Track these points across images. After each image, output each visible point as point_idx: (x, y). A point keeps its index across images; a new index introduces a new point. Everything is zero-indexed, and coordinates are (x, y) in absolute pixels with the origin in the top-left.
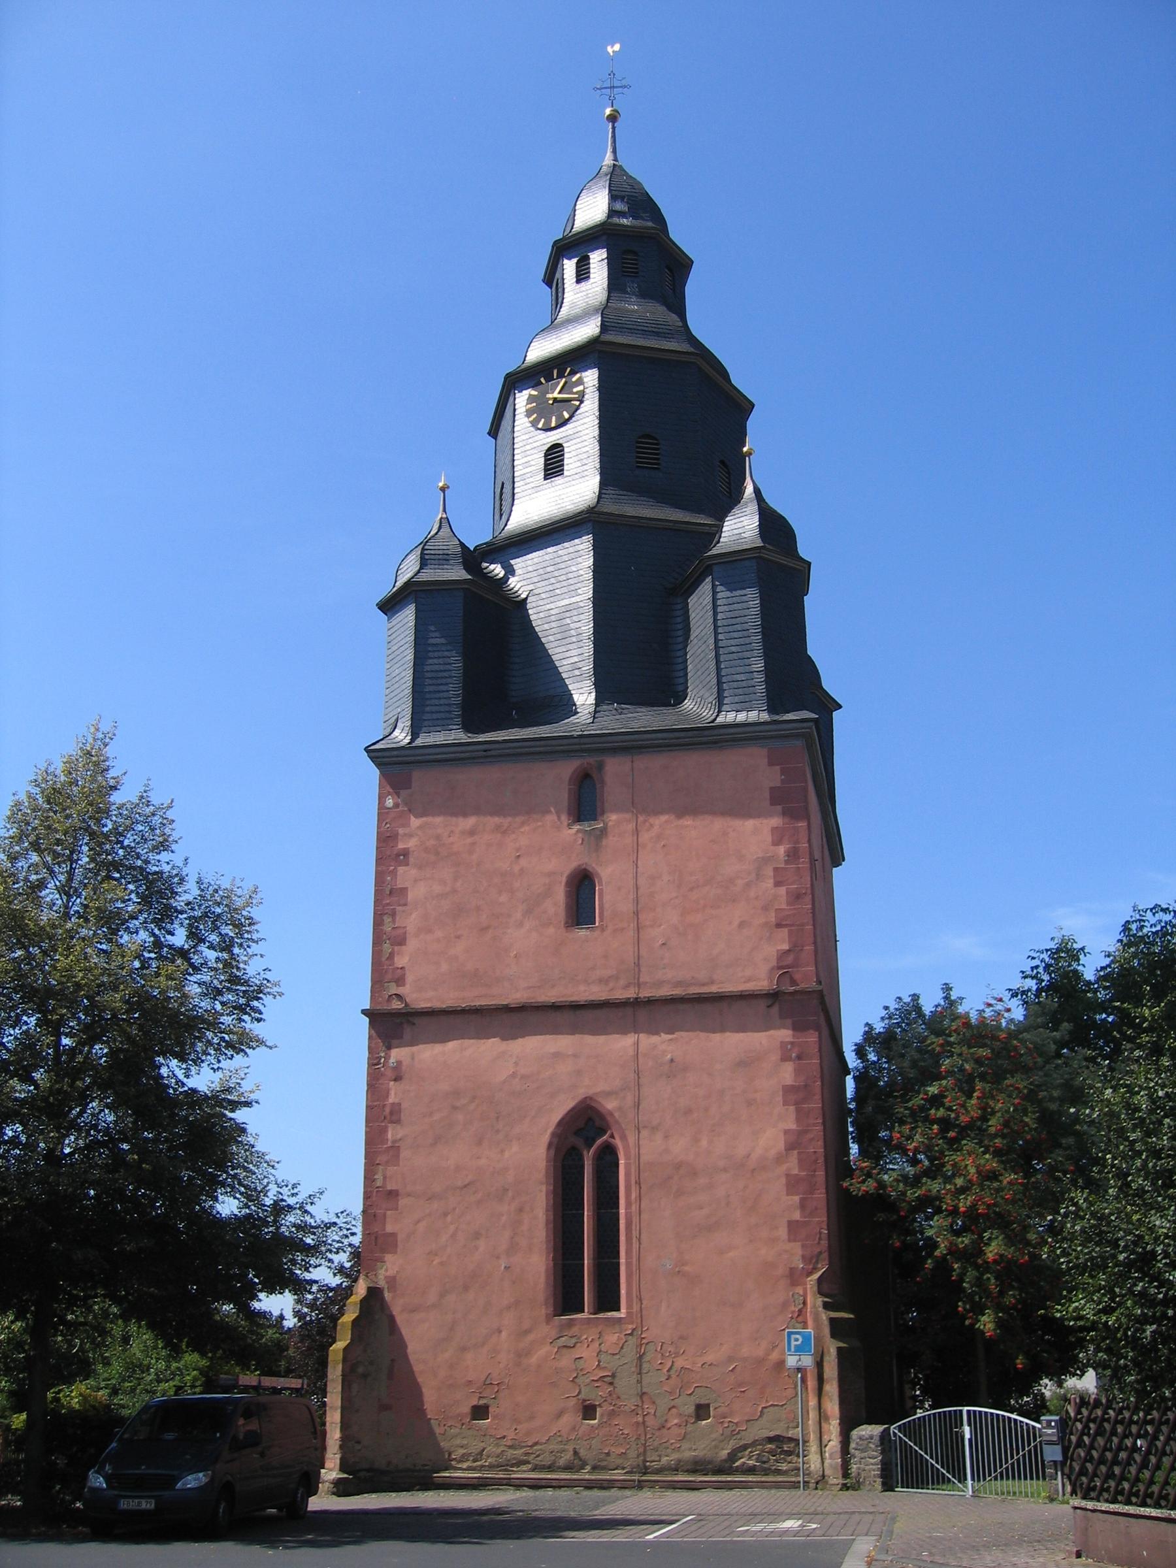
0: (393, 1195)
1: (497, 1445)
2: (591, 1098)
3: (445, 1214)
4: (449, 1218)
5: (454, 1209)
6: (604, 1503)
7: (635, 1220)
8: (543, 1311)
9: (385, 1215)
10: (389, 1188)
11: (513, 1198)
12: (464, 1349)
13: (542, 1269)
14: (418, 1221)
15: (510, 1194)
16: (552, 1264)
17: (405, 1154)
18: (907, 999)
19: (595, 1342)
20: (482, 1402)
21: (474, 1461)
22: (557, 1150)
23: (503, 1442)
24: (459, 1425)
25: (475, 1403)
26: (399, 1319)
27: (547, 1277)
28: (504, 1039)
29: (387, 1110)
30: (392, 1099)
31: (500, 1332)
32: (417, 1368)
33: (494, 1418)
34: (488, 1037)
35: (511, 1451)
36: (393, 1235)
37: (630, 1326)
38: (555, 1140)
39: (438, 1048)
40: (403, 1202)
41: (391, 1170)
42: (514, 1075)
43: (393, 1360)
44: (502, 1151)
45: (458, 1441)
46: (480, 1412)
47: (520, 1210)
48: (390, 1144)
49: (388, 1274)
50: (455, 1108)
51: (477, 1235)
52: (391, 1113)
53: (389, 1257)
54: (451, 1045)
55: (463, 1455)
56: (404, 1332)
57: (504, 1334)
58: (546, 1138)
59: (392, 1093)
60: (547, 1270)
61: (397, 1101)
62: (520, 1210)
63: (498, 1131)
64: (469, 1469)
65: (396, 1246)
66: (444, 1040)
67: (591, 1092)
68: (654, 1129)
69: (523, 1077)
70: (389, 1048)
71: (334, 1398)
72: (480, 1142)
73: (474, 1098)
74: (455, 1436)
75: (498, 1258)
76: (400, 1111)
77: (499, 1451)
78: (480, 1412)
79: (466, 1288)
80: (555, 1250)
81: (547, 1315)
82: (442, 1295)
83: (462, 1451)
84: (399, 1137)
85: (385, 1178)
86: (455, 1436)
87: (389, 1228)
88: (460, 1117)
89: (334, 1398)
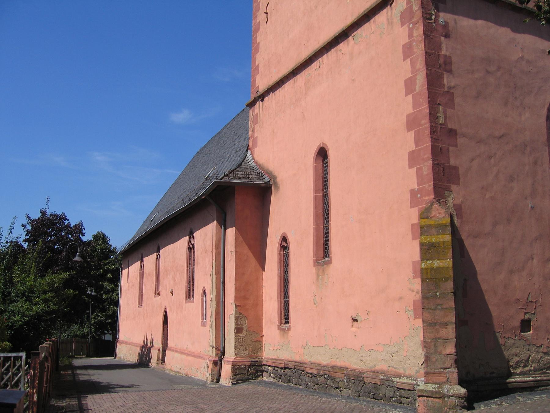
0: (452, 133)
1: (538, 352)
3: (490, 157)
4: (493, 160)
5: (495, 154)
6: (94, 374)
9: (448, 151)
10: (450, 126)
12: (511, 272)
14: (473, 160)
15: (528, 149)
17: (457, 100)
18: (83, 231)
19: (141, 309)
20: (527, 317)
21: (525, 366)
23: (541, 349)
24: (513, 337)
25: (523, 318)
26: (467, 243)
28: (514, 31)
29: (442, 60)
30: (444, 52)
31: (533, 259)
32: (484, 287)
33: (534, 330)
34: (502, 25)
35: (546, 357)
36: (456, 168)
39: (471, 22)
40: (461, 141)
41: (449, 111)
42: (522, 58)
43: (465, 280)
44: (520, 115)
45: (513, 351)
46: (526, 325)
48: (446, 89)
49: (455, 202)
50: (488, 72)
51: (511, 179)
52: (445, 63)
53: (453, 187)
54: (480, 22)
55: (517, 362)
56: (471, 255)
57: (535, 261)
59: (444, 46)
61: (448, 54)
62: (535, 163)
64: (522, 374)
65: (459, 179)
66: (476, 19)
69: (528, 61)
70: (438, 9)
72: (506, 104)
73: (499, 68)
74: (511, 347)
75: (526, 198)
76: (450, 63)
77: (539, 357)
78: (526, 325)
79: (509, 221)
82: (495, 225)
83: (516, 359)
84: (452, 84)
85: (446, 117)
86: (511, 347)
87: (453, 162)
88: (491, 80)
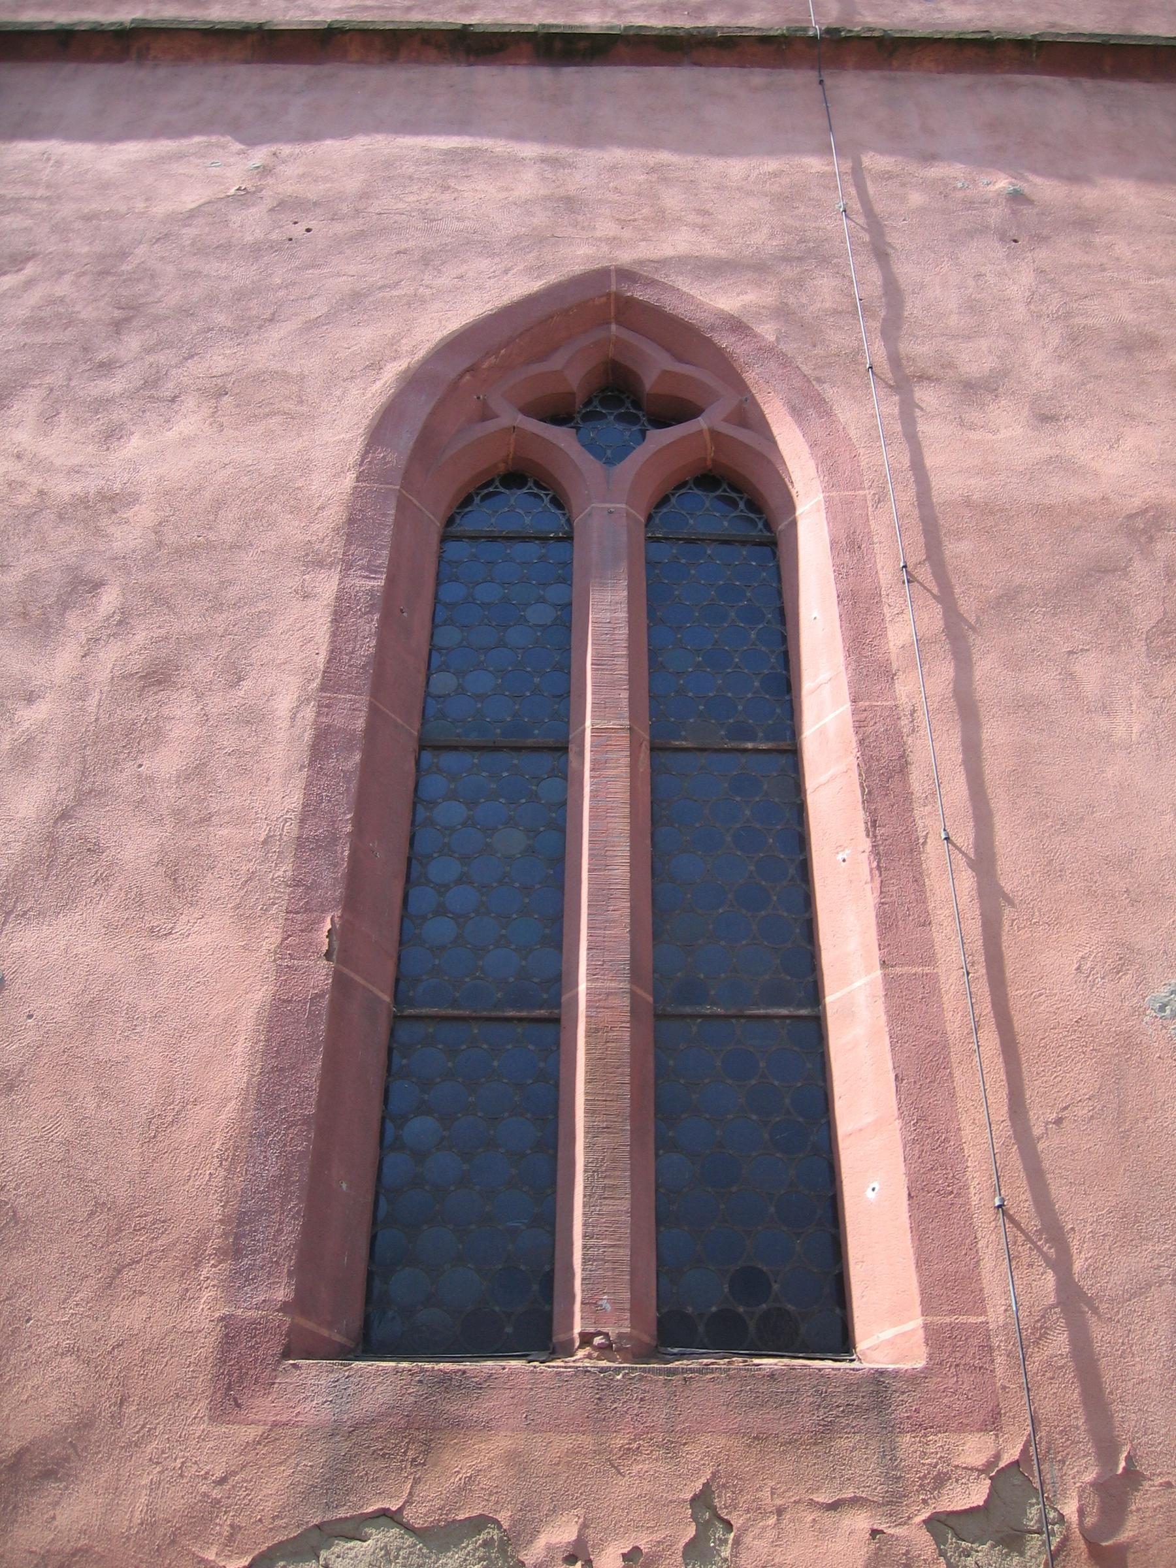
2: (626, 275)
7: (934, 751)
8: (206, 1307)
11: (123, 621)
13: (227, 1075)
15: (109, 600)
16: (320, 975)
22: (426, 447)
27: (266, 1096)
37: (974, 1450)
38: (421, 409)
47: (158, 677)
58: (372, 393)
60: (278, 1014)
62: (158, 677)
63: (107, 367)
67: (625, 257)
68: (975, 390)
71: (607, 618)
80: (355, 894)
81: (232, 1334)
89: (607, 618)
